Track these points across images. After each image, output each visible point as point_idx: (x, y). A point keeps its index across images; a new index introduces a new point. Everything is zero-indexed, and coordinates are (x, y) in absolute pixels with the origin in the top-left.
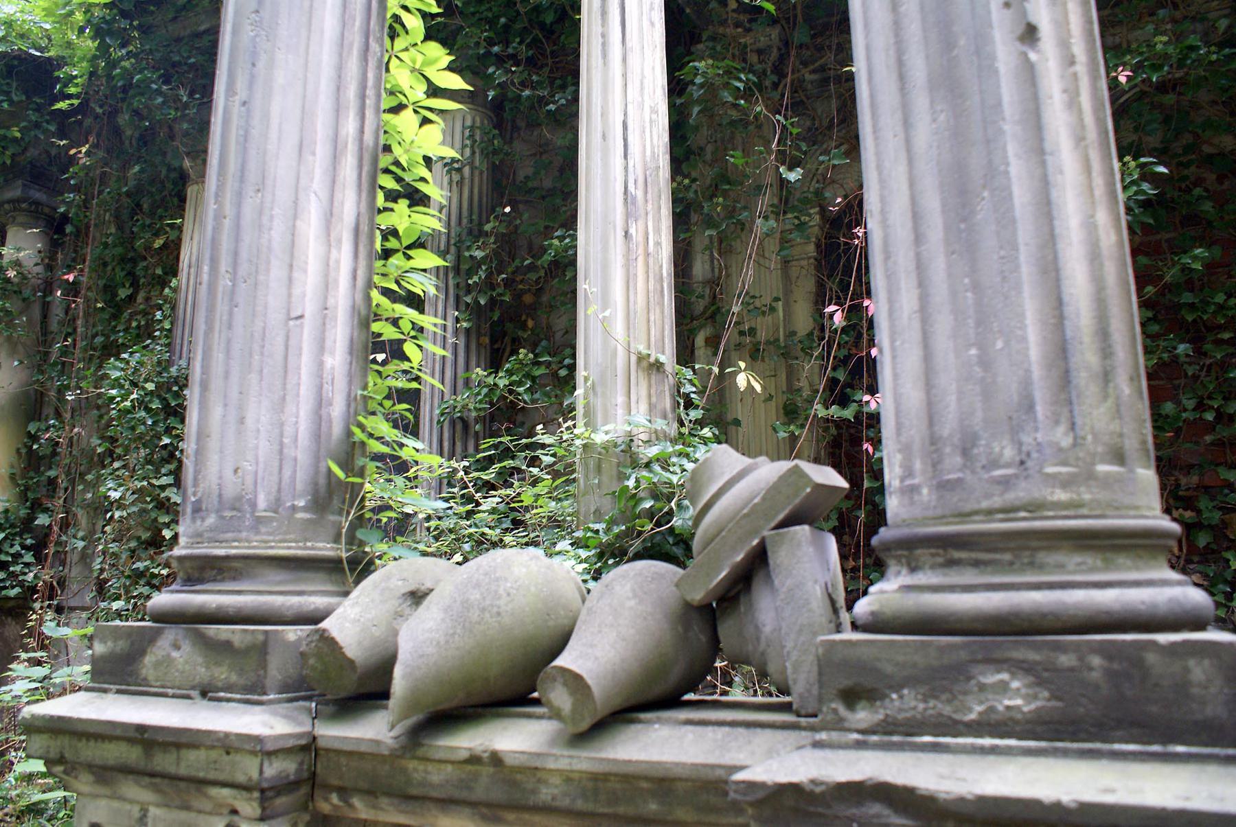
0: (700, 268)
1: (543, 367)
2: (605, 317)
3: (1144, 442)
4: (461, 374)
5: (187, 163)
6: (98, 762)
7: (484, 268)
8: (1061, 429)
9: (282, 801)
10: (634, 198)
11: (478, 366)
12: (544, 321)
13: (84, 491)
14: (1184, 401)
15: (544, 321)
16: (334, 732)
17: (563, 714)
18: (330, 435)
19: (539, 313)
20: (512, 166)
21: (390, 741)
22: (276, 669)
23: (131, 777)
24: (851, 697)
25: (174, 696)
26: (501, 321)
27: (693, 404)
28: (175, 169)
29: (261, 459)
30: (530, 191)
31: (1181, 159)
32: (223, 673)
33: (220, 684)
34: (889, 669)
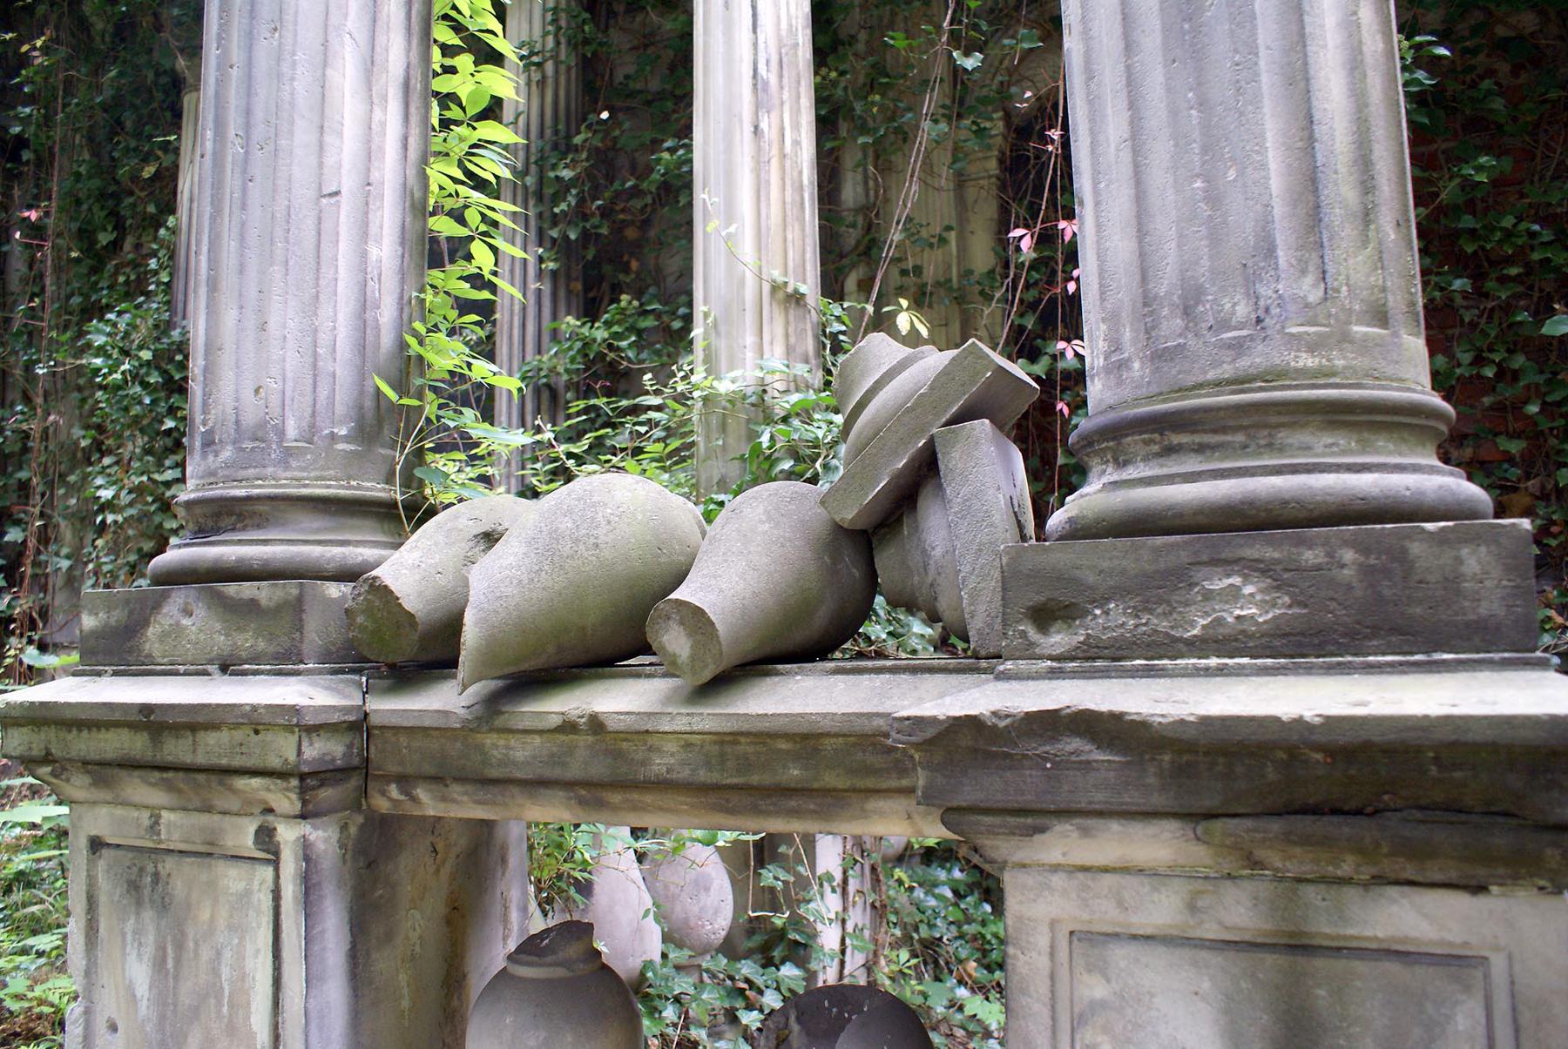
0: (851, 192)
1: (651, 317)
2: (729, 236)
3: (1413, 304)
4: (547, 324)
5: (181, 63)
6: (93, 756)
7: (574, 191)
8: (1309, 280)
9: (327, 794)
10: (766, 84)
11: (568, 314)
12: (652, 262)
13: (66, 496)
14: (1459, 355)
15: (652, 262)
16: (389, 706)
17: (679, 662)
18: (378, 346)
19: (646, 250)
20: (608, 60)
21: (461, 712)
22: (316, 631)
23: (137, 773)
24: (1044, 616)
25: (186, 674)
26: (597, 263)
27: (842, 348)
28: (165, 72)
29: (289, 375)
30: (632, 95)
31: (1468, 43)
32: (247, 641)
33: (244, 654)
34: (1091, 579)
